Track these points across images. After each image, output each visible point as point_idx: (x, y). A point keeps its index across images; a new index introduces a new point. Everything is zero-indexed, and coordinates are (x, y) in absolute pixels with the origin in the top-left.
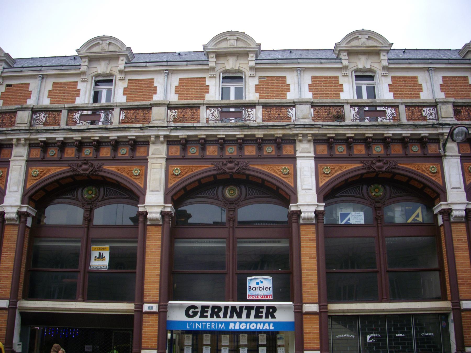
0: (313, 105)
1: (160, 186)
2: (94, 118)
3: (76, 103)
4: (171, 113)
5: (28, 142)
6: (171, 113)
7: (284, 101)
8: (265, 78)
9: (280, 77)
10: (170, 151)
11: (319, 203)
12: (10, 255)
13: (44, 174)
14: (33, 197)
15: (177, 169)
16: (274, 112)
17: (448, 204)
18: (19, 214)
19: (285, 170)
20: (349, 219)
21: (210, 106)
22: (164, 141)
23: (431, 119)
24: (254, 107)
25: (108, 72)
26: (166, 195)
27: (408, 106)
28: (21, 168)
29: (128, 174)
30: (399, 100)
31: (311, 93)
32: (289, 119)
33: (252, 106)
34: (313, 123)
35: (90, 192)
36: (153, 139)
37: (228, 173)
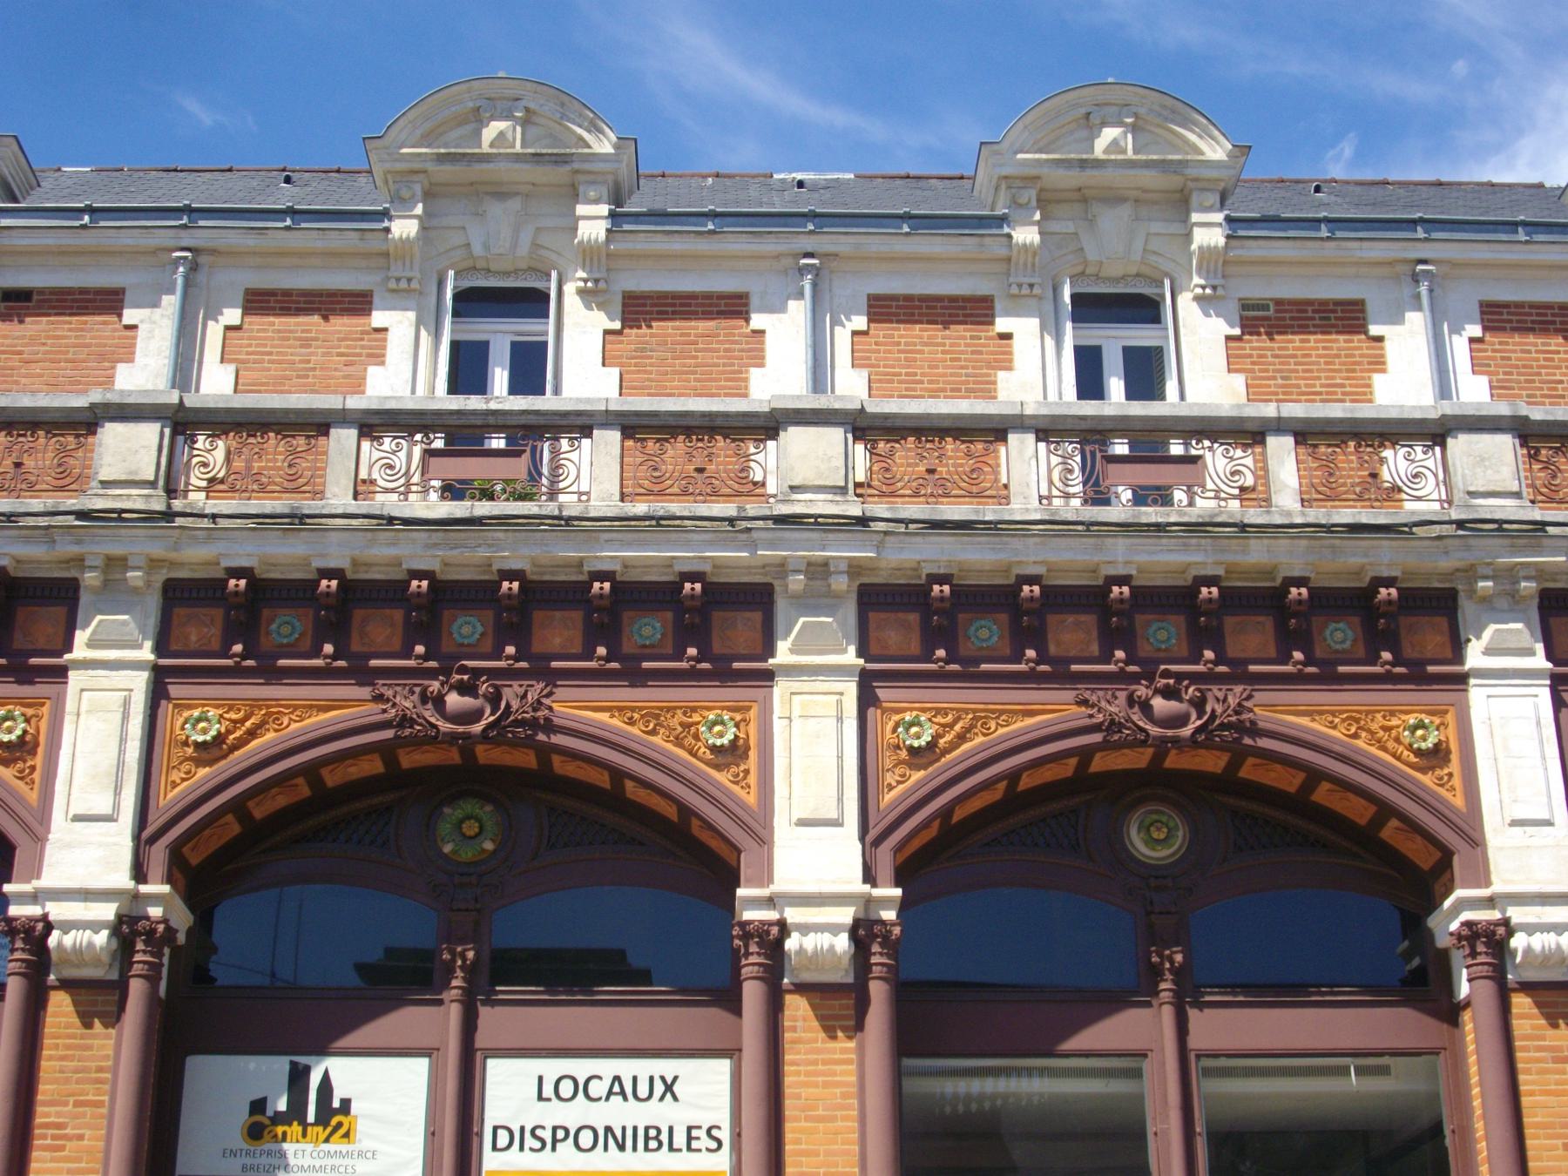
1: (840, 800)
3: (370, 391)
4: (376, 455)
6: (376, 455)
7: (1363, 411)
8: (1266, 308)
9: (1338, 303)
10: (873, 634)
11: (874, 885)
12: (81, 1137)
13: (252, 734)
15: (917, 718)
17: (1490, 902)
19: (1420, 732)
21: (373, 424)
22: (148, 584)
23: (1419, 499)
24: (586, 431)
26: (143, 841)
27: (1305, 434)
28: (126, 704)
29: (678, 742)
30: (1269, 410)
31: (1483, 381)
32: (756, 488)
33: (581, 424)
35: (470, 828)
36: (797, 581)
37: (453, 737)
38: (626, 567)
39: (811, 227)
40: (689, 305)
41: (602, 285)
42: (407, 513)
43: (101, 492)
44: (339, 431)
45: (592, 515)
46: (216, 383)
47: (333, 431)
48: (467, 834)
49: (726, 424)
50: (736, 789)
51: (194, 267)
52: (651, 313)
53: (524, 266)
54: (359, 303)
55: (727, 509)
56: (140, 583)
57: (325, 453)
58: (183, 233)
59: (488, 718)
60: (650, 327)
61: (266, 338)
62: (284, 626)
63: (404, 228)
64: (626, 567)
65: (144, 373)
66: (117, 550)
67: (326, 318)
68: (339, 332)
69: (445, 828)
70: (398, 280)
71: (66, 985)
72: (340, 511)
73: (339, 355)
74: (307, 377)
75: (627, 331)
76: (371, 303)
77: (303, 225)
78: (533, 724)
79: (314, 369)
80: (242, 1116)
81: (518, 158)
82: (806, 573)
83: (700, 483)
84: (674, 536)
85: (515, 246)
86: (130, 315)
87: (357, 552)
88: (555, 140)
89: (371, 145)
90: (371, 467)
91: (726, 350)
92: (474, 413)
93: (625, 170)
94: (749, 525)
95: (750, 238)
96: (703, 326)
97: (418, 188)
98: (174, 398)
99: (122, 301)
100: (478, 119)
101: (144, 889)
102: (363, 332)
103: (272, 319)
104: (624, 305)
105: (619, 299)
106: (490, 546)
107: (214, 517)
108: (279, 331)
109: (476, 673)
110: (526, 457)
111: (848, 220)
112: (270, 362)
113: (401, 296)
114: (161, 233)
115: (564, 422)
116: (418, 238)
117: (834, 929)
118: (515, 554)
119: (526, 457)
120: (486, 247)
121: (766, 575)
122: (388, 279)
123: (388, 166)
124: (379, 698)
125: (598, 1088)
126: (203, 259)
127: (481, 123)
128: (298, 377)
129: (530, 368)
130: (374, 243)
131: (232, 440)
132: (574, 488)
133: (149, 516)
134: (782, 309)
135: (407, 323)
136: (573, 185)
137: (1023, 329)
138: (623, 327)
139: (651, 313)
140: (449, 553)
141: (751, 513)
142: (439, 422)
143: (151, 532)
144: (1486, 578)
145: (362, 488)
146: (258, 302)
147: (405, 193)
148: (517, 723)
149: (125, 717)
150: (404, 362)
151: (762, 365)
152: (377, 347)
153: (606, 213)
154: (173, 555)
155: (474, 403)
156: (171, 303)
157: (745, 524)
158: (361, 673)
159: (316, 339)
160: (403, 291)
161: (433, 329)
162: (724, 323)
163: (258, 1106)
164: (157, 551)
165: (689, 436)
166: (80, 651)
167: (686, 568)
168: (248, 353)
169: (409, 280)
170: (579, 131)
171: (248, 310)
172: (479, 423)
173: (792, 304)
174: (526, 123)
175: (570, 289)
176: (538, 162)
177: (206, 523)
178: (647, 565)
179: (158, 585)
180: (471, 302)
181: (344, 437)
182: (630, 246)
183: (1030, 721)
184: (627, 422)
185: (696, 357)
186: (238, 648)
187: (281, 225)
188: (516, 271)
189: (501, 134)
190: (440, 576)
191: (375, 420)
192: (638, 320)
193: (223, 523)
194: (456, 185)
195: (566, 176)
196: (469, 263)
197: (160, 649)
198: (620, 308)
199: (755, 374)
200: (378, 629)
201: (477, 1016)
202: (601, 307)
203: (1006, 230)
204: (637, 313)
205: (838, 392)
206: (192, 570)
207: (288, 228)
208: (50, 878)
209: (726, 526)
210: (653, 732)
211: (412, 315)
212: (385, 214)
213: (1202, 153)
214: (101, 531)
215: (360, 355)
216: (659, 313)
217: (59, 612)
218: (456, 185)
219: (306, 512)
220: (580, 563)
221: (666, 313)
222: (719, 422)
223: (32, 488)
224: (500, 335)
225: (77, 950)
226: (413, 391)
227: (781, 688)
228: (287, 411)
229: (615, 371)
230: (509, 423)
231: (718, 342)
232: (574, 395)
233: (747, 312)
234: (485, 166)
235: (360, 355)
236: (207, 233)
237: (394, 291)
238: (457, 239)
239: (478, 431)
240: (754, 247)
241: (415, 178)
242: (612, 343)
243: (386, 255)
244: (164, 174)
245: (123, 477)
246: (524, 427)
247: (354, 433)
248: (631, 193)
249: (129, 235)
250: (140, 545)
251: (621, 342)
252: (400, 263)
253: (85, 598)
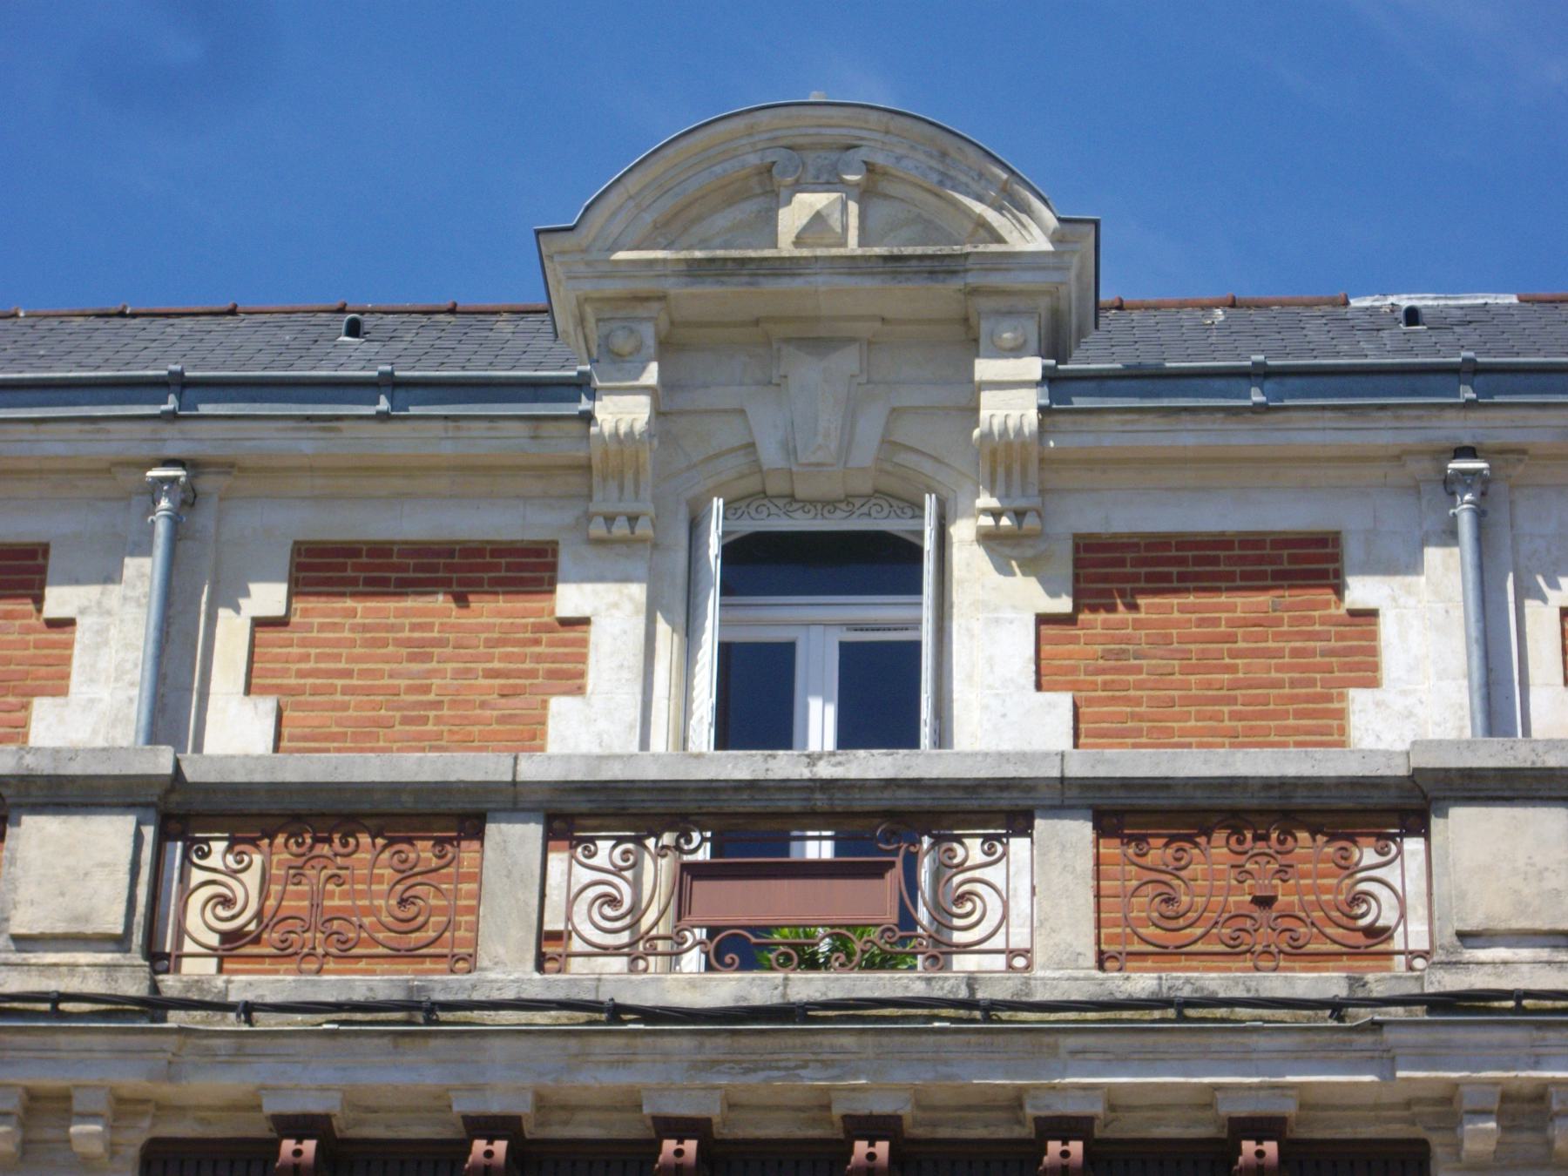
0: (1121, 812)
3: (553, 747)
4: (583, 876)
6: (586, 876)
16: (1213, 869)
21: (575, 812)
22: (113, 1149)
24: (1020, 823)
33: (1007, 807)
38: (732, 1106)
39: (1468, 394)
40: (1214, 561)
41: (1031, 522)
42: (649, 997)
43: (16, 958)
44: (504, 826)
45: (1039, 996)
46: (237, 734)
47: (491, 828)
49: (1315, 804)
51: (189, 500)
52: (1135, 578)
53: (866, 487)
54: (530, 568)
55: (1328, 982)
56: (97, 1148)
57: (477, 877)
58: (169, 430)
60: (1133, 607)
61: (338, 643)
63: (621, 413)
64: (1112, 1107)
65: (91, 711)
66: (47, 1079)
67: (461, 600)
68: (488, 628)
70: (610, 519)
72: (509, 995)
73: (490, 674)
74: (424, 720)
75: (1084, 616)
76: (553, 567)
77: (414, 410)
79: (437, 705)
81: (853, 265)
82: (1500, 1116)
83: (1265, 930)
84: (1217, 1041)
85: (846, 447)
86: (59, 600)
87: (548, 1081)
88: (929, 229)
89: (551, 245)
90: (571, 903)
91: (1296, 653)
92: (785, 785)
93: (1071, 284)
94: (1379, 1015)
95: (1342, 420)
96: (1245, 603)
97: (648, 333)
98: (161, 762)
99: (42, 570)
100: (769, 188)
102: (538, 628)
103: (349, 603)
104: (1078, 563)
105: (1068, 547)
106: (825, 1064)
107: (248, 1010)
108: (365, 628)
110: (895, 876)
111: (351, 392)
112: (346, 691)
113: (614, 552)
114: (123, 432)
115: (973, 804)
116: (650, 433)
118: (878, 1082)
119: (895, 876)
120: (789, 450)
121: (1412, 1122)
122: (589, 517)
123: (587, 287)
126: (207, 483)
128: (406, 721)
129: (885, 694)
130: (561, 446)
131: (282, 850)
132: (998, 942)
133: (114, 1008)
134: (1411, 565)
135: (628, 607)
136: (966, 320)
137: (607, 607)
138: (1077, 608)
139: (1135, 578)
140: (741, 1081)
141: (1378, 991)
142: (711, 807)
143: (122, 1041)
144: (86, 1117)
145: (549, 947)
146: (320, 569)
147: (622, 342)
150: (627, 686)
151: (1373, 683)
152: (566, 658)
153: (1037, 374)
154: (165, 1090)
155: (781, 765)
156: (143, 573)
157: (1365, 1015)
159: (441, 643)
160: (623, 541)
161: (681, 620)
162: (1289, 597)
164: (131, 1079)
165: (1237, 831)
167: (1243, 1109)
168: (301, 674)
169: (633, 519)
170: (979, 208)
172: (795, 806)
173: (1433, 555)
174: (865, 194)
175: (963, 532)
176: (895, 274)
177: (231, 1023)
178: (1161, 1102)
179: (133, 1152)
180: (759, 563)
181: (515, 840)
182: (1088, 440)
184: (1105, 802)
185: (1232, 669)
187: (369, 410)
188: (848, 499)
189: (818, 218)
190: (721, 1132)
191: (581, 804)
192: (1108, 593)
193: (266, 1022)
194: (725, 325)
195: (956, 302)
196: (751, 484)
198: (1068, 570)
199: (1359, 700)
202: (1029, 567)
203: (585, 405)
204: (1105, 578)
205: (1537, 731)
206: (202, 1121)
207: (383, 417)
209: (1324, 1019)
211: (638, 591)
212: (581, 386)
213: (1000, 240)
214: (20, 1040)
215: (532, 674)
216: (1150, 577)
218: (725, 325)
219: (440, 996)
220: (1015, 1102)
221: (1166, 577)
222: (1299, 800)
223: (1297, 954)
224: (819, 630)
226: (644, 743)
228: (395, 789)
229: (1064, 700)
230: (857, 806)
231: (1278, 636)
233: (1338, 574)
234: (785, 284)
235: (532, 674)
236: (215, 430)
237: (600, 542)
238: (728, 434)
239: (775, 825)
240: (1165, 440)
241: (641, 311)
242: (1056, 641)
243: (586, 468)
244: (100, 323)
245: (60, 928)
246: (888, 814)
247: (535, 831)
248: (1082, 333)
249: (58, 436)
250: (97, 1068)
251: (1074, 640)
252: (613, 485)
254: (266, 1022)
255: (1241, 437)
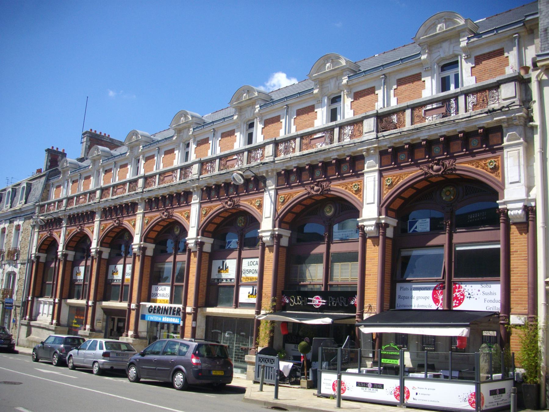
1: (520, 176)
2: (443, 110)
3: (423, 97)
5: (378, 151)
13: (398, 181)
14: (391, 207)
18: (378, 225)
20: (416, 228)
25: (451, 53)
26: (380, 207)
28: (374, 178)
29: (483, 169)
34: (442, 120)
48: (448, 195)
50: (496, 178)
59: (442, 170)
62: (474, 142)
69: (443, 195)
71: (514, 224)
78: (451, 169)
80: (217, 269)
100: (435, 25)
101: (381, 217)
109: (439, 160)
117: (518, 209)
124: (421, 169)
125: (255, 263)
127: (436, 26)
146: (401, 82)
148: (449, 170)
149: (375, 181)
150: (429, 88)
156: (515, 49)
158: (417, 165)
163: (219, 268)
166: (505, 143)
171: (165, 154)
183: (411, 175)
186: (410, 160)
189: (440, 27)
193: (386, 137)
197: (381, 166)
200: (419, 154)
201: (453, 236)
208: (507, 198)
210: (478, 167)
217: (499, 134)
218: (432, 44)
222: (490, 86)
225: (514, 215)
227: (137, 215)
232: (467, 85)
253: (504, 130)
254: (386, 137)
255: (299, 99)
